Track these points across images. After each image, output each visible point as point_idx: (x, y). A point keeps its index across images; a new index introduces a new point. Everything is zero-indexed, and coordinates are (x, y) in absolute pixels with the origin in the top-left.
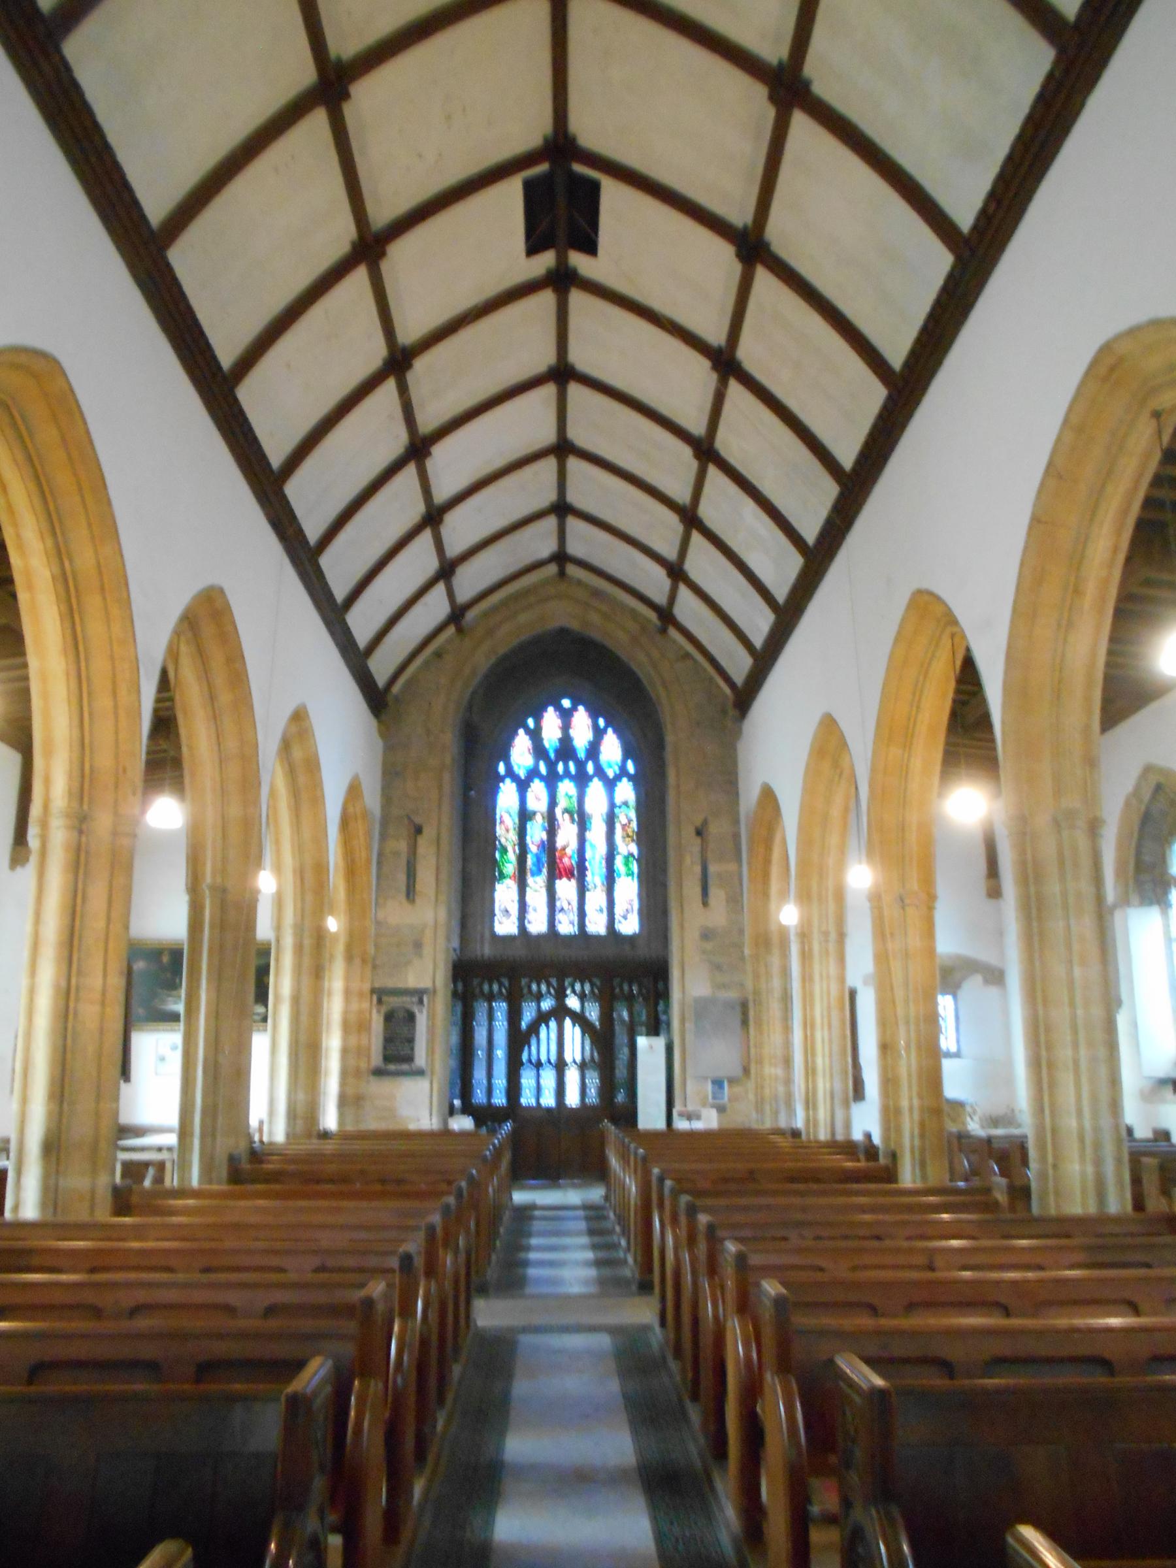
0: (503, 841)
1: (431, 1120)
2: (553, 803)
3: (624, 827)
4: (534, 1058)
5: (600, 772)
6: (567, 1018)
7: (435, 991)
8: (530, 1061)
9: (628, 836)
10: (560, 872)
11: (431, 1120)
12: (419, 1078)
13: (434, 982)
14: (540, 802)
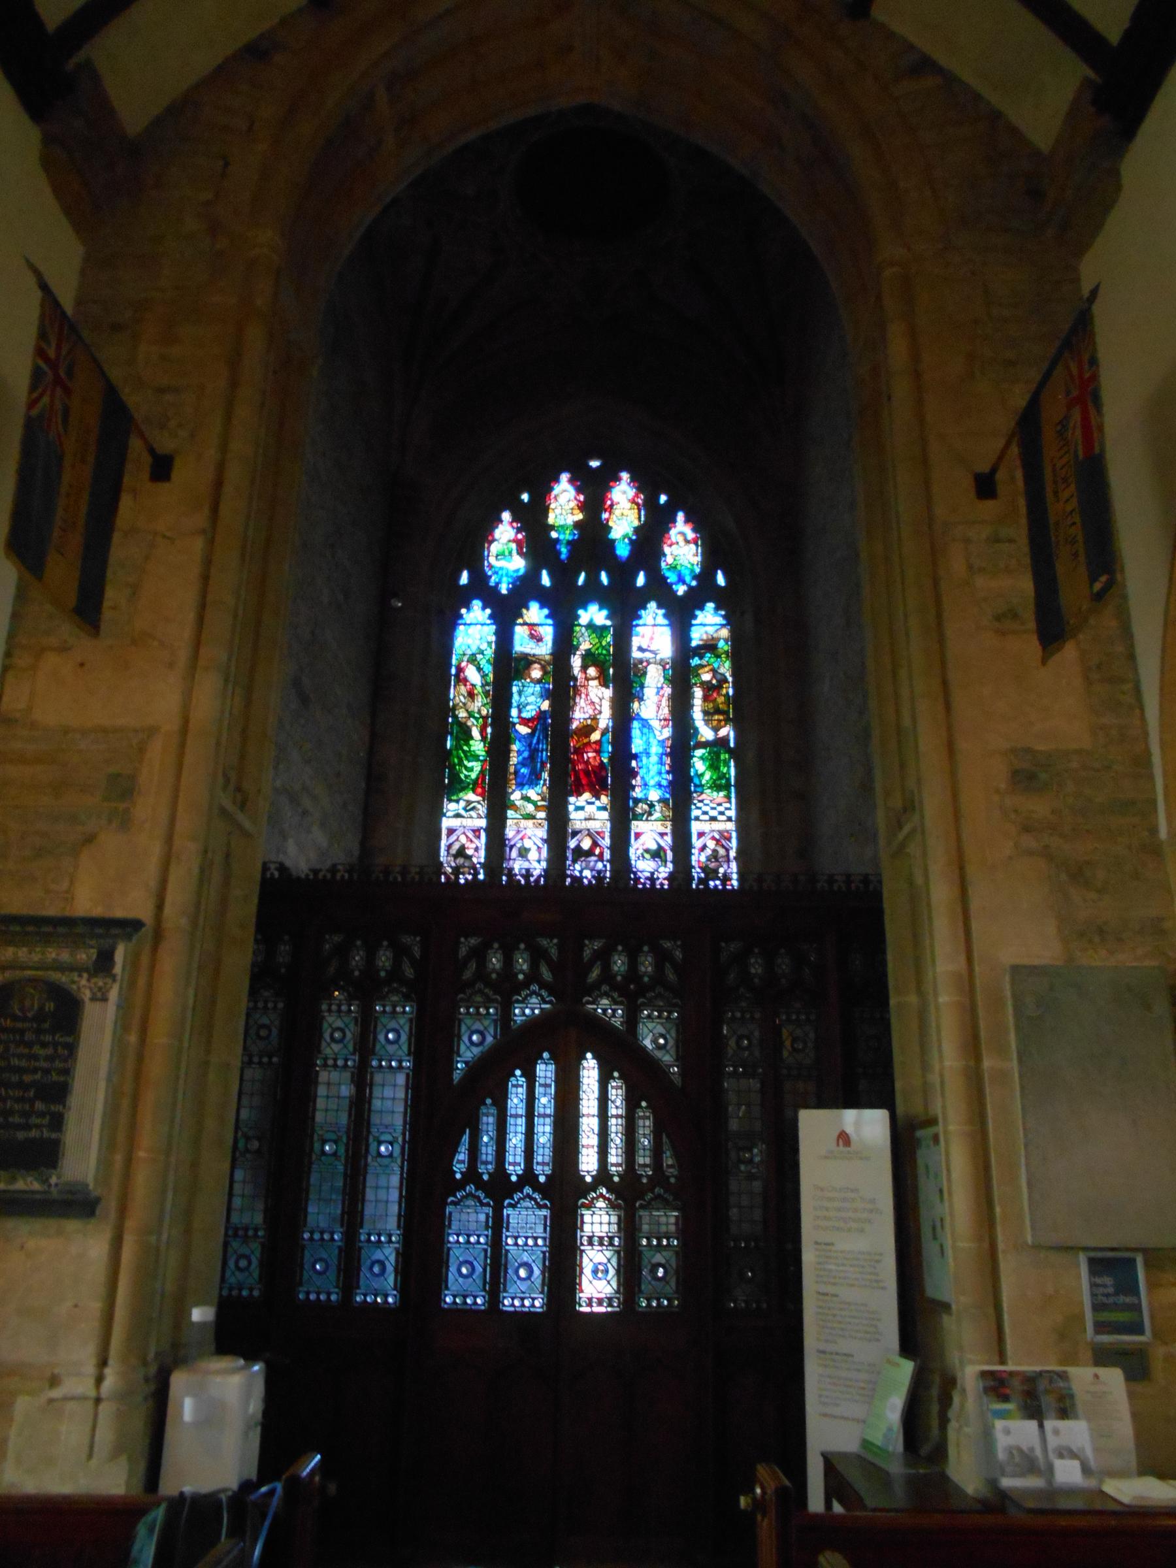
0: (462, 714)
1: (99, 1380)
2: (564, 644)
3: (708, 688)
4: (486, 1170)
5: (659, 590)
6: (564, 477)
7: (158, 935)
8: (472, 1174)
9: (718, 711)
10: (578, 779)
11: (99, 1380)
12: (72, 1225)
13: (160, 907)
14: (540, 644)
